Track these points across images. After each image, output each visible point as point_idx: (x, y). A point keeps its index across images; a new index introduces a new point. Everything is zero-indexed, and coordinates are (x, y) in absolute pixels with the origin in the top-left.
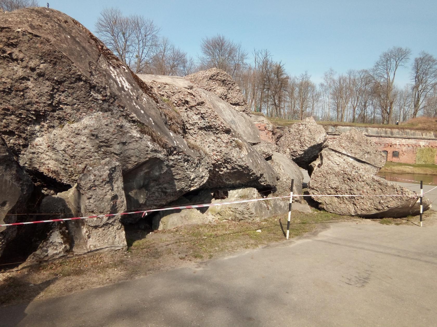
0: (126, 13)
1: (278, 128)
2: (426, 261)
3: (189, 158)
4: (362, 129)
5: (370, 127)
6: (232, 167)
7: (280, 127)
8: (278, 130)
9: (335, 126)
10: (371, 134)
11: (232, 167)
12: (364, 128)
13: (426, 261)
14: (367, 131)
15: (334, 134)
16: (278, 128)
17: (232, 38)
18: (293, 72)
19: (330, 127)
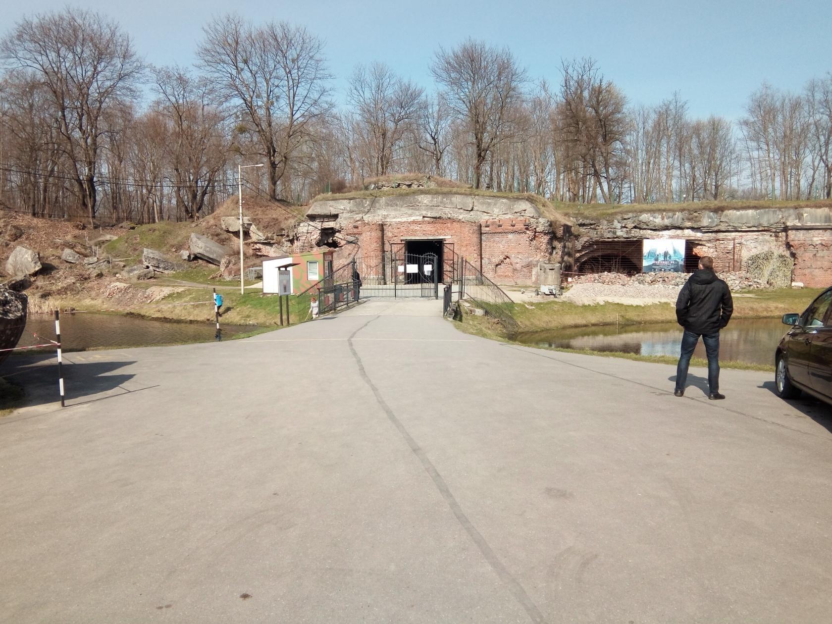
0: (255, 20)
1: (581, 225)
2: (594, 349)
3: (413, 269)
4: (786, 214)
5: (807, 206)
6: (84, 60)
7: (587, 222)
8: (582, 230)
9: (719, 210)
10: (809, 224)
11: (84, 60)
12: (792, 211)
13: (594, 349)
14: (799, 217)
15: (716, 229)
16: (581, 225)
17: (492, 40)
18: (640, 96)
19: (707, 213)
